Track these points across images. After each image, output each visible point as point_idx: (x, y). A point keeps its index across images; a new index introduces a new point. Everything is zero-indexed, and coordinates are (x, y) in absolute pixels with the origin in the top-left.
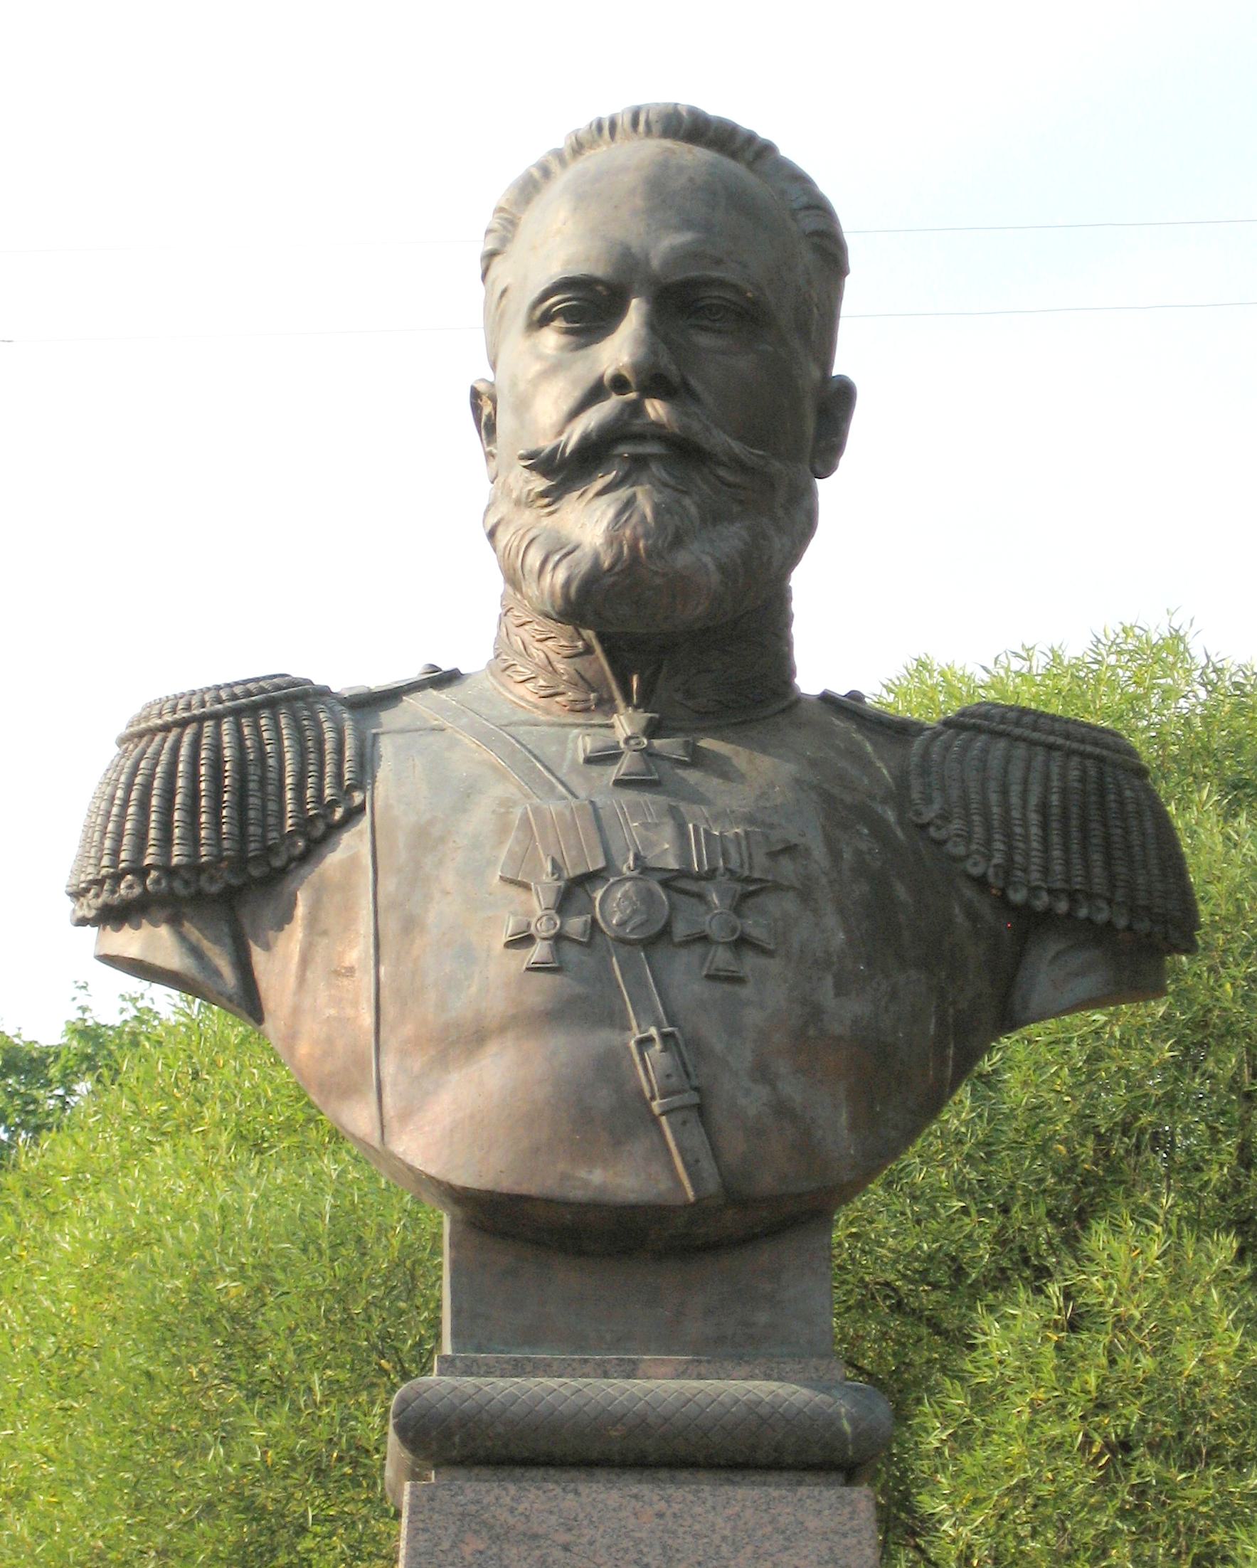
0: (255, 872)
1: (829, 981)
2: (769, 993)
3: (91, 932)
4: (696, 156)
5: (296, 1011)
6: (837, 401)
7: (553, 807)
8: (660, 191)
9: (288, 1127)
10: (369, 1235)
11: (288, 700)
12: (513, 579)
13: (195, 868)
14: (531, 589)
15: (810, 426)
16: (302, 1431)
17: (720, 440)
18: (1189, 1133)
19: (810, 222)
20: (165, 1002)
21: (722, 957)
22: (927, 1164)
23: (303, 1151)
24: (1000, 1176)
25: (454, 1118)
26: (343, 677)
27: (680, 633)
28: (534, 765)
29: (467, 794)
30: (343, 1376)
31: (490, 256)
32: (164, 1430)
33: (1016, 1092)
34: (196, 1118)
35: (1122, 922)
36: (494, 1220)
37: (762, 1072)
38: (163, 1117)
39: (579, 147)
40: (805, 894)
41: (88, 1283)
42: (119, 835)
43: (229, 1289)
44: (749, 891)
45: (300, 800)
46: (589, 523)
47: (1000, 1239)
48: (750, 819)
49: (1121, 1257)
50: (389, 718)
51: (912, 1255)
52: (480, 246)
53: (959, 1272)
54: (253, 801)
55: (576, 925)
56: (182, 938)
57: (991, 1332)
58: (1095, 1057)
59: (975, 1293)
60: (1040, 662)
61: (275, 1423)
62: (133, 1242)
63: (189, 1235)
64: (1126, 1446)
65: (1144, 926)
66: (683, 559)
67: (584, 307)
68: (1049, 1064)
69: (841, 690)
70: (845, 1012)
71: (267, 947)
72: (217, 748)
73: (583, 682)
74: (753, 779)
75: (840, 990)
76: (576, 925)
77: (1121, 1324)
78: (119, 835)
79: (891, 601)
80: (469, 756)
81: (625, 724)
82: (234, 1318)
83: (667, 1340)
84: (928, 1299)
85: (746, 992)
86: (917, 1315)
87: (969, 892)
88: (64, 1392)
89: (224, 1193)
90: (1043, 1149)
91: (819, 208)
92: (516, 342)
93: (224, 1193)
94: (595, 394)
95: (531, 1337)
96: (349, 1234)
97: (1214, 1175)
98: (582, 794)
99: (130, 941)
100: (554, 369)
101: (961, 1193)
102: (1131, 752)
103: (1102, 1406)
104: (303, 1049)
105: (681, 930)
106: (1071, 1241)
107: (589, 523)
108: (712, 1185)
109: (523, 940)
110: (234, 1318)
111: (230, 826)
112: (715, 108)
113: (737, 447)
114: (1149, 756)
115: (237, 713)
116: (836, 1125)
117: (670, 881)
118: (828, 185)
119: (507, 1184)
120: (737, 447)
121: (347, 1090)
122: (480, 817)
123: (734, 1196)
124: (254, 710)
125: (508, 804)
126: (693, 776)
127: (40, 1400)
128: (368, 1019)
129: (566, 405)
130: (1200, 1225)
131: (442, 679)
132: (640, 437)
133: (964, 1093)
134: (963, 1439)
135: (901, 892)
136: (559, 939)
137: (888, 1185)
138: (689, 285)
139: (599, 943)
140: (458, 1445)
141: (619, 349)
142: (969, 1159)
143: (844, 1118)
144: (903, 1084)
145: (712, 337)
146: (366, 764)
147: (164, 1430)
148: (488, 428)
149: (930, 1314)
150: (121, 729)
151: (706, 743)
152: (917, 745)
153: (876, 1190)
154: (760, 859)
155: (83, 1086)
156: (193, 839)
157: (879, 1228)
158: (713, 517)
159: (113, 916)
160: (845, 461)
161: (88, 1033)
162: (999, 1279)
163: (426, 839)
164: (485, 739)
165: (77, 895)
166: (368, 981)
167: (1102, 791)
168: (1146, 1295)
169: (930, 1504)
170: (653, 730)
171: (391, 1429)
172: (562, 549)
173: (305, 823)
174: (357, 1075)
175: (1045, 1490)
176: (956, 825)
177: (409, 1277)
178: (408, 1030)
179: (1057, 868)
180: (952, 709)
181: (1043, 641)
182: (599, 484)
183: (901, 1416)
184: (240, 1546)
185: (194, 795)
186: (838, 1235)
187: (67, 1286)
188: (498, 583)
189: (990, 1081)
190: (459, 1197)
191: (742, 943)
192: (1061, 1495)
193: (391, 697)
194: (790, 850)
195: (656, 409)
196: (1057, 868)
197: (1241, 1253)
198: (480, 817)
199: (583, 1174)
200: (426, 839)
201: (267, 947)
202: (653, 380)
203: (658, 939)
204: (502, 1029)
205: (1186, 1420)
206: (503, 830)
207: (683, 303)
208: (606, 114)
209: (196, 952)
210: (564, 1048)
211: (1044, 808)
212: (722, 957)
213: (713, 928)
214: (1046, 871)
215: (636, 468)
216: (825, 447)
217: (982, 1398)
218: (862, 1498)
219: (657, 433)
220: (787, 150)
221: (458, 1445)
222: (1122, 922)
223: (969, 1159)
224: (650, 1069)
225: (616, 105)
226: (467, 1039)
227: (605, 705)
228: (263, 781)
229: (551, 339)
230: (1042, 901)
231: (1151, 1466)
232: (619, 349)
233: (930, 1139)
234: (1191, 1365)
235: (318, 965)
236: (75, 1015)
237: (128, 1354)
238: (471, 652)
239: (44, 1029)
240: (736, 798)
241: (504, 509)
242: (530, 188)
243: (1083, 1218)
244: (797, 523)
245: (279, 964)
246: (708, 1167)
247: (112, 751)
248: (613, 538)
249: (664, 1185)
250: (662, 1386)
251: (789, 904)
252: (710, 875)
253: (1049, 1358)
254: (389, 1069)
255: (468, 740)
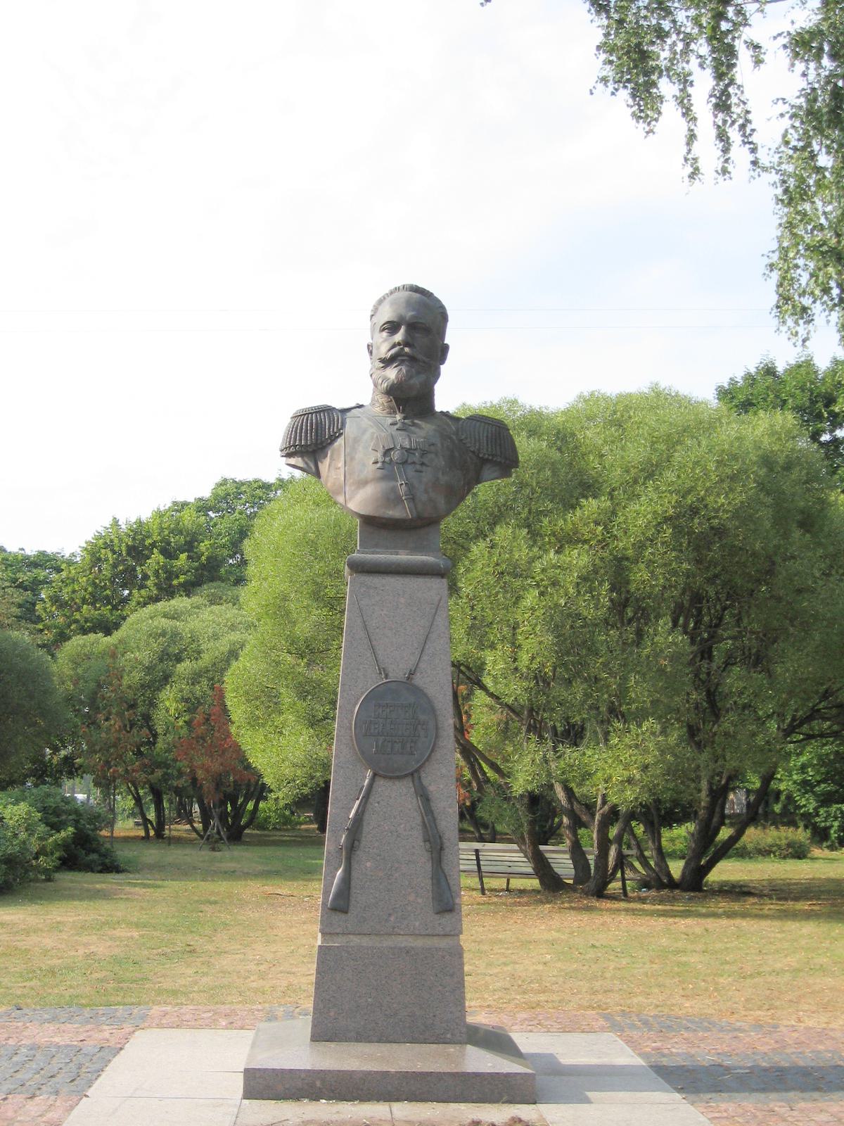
0: (320, 446)
1: (441, 473)
2: (427, 476)
3: (284, 458)
4: (417, 295)
5: (328, 476)
6: (445, 349)
7: (383, 434)
8: (409, 303)
9: (324, 501)
10: (342, 525)
11: (327, 410)
12: (375, 385)
13: (306, 446)
14: (379, 387)
15: (440, 354)
16: (327, 567)
17: (420, 357)
18: (519, 506)
19: (441, 310)
20: (298, 474)
21: (418, 467)
22: (461, 512)
23: (328, 507)
24: (477, 515)
25: (360, 500)
26: (339, 404)
27: (410, 400)
28: (378, 424)
29: (365, 431)
30: (336, 555)
31: (372, 316)
32: (297, 566)
33: (481, 497)
34: (304, 499)
35: (503, 461)
36: (370, 522)
37: (426, 491)
38: (298, 498)
39: (391, 293)
40: (436, 455)
41: (281, 534)
42: (291, 438)
43: (312, 536)
44: (424, 453)
45: (329, 431)
46: (392, 373)
47: (477, 528)
48: (425, 438)
49: (503, 533)
50: (348, 414)
51: (457, 532)
52: (370, 313)
53: (468, 535)
54: (319, 432)
55: (387, 459)
56: (304, 460)
57: (474, 548)
58: (499, 489)
59: (471, 539)
60: (488, 405)
61: (321, 565)
62: (291, 525)
63: (303, 524)
64: (502, 573)
65: (507, 462)
66: (412, 382)
67: (392, 327)
68: (487, 491)
69: (445, 411)
70: (444, 479)
71: (322, 462)
72: (312, 420)
73: (391, 408)
74: (426, 429)
75: (443, 474)
76: (387, 459)
77: (502, 547)
78: (291, 438)
79: (453, 393)
80: (365, 422)
81: (398, 417)
82: (312, 541)
83: (405, 547)
84: (461, 541)
85: (423, 474)
86: (458, 544)
87: (471, 454)
88: (276, 557)
89: (311, 515)
90: (487, 509)
91: (442, 307)
92: (377, 335)
93: (311, 515)
94: (394, 346)
95: (376, 546)
96: (337, 524)
97: (523, 516)
98: (389, 431)
99: (292, 461)
100: (385, 340)
101: (469, 518)
102: (506, 425)
103: (497, 565)
104: (329, 484)
105: (409, 461)
106: (492, 529)
107: (392, 373)
108: (415, 515)
109: (376, 462)
110: (312, 541)
111: (314, 436)
112: (420, 285)
113: (424, 358)
114: (511, 426)
115: (316, 412)
116: (442, 503)
117: (408, 450)
118: (444, 303)
119: (371, 514)
120: (424, 358)
121: (338, 493)
122: (367, 436)
123: (419, 517)
124: (320, 412)
125: (373, 433)
126: (413, 428)
127: (270, 558)
128: (343, 479)
129: (388, 348)
130: (519, 527)
131: (360, 406)
132: (403, 356)
133: (469, 497)
134: (468, 570)
135: (457, 454)
136: (383, 462)
137: (453, 516)
138: (414, 323)
139: (391, 464)
140: (360, 568)
141: (399, 337)
142: (471, 511)
143: (443, 502)
144: (456, 495)
145: (418, 334)
146: (343, 424)
147: (297, 566)
148: (371, 353)
149: (461, 544)
150: (291, 415)
151: (416, 421)
152: (461, 423)
153: (450, 518)
154: (427, 446)
155: (279, 492)
156: (306, 439)
157: (450, 525)
158: (418, 373)
159: (289, 455)
160: (447, 362)
161: (281, 480)
162: (476, 537)
163: (356, 440)
164: (369, 419)
165: (282, 451)
166: (343, 470)
167: (499, 433)
168: (508, 541)
169: (460, 585)
170: (405, 418)
171: (346, 566)
172: (385, 379)
173: (330, 436)
174: (340, 490)
175: (485, 582)
176: (469, 440)
177: (350, 534)
178: (351, 481)
179: (490, 450)
180: (469, 414)
181: (488, 400)
182: (395, 365)
183: (454, 566)
184: (313, 591)
185: (307, 430)
186: (441, 527)
187: (277, 534)
188: (372, 386)
189: (475, 494)
190: (361, 516)
191: (423, 464)
192: (488, 583)
193: (349, 410)
194: (433, 444)
195: (407, 349)
196: (490, 450)
197: (528, 533)
198: (367, 436)
199: (388, 512)
200: (356, 440)
201: (322, 462)
202: (406, 344)
203: (404, 463)
204: (371, 481)
205: (515, 568)
206: (372, 438)
207: (413, 327)
208: (397, 286)
209: (306, 463)
210: (383, 486)
211: (487, 437)
212: (418, 467)
213: (417, 461)
214: (487, 451)
215: (402, 362)
216: (443, 360)
217: (472, 562)
218: (445, 581)
219: (406, 354)
220: (436, 295)
221: (360, 568)
222: (503, 461)
223: (471, 511)
224: (402, 490)
225: (399, 284)
226: (364, 483)
227: (395, 413)
228: (321, 428)
229: (385, 334)
230: (486, 456)
231: (507, 578)
232: (399, 337)
233: (462, 506)
234: (517, 557)
235: (333, 467)
236: (278, 476)
237: (289, 549)
238: (366, 400)
239: (270, 478)
240: (422, 433)
241: (374, 370)
242: (381, 302)
243: (495, 524)
244: (436, 375)
245: (324, 466)
246: (414, 511)
247: (289, 420)
248: (397, 377)
249: (405, 515)
250: (403, 557)
251: (433, 456)
252: (416, 449)
253: (486, 554)
254: (347, 489)
255: (366, 420)
